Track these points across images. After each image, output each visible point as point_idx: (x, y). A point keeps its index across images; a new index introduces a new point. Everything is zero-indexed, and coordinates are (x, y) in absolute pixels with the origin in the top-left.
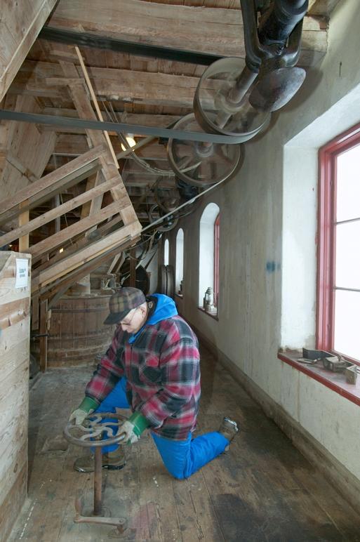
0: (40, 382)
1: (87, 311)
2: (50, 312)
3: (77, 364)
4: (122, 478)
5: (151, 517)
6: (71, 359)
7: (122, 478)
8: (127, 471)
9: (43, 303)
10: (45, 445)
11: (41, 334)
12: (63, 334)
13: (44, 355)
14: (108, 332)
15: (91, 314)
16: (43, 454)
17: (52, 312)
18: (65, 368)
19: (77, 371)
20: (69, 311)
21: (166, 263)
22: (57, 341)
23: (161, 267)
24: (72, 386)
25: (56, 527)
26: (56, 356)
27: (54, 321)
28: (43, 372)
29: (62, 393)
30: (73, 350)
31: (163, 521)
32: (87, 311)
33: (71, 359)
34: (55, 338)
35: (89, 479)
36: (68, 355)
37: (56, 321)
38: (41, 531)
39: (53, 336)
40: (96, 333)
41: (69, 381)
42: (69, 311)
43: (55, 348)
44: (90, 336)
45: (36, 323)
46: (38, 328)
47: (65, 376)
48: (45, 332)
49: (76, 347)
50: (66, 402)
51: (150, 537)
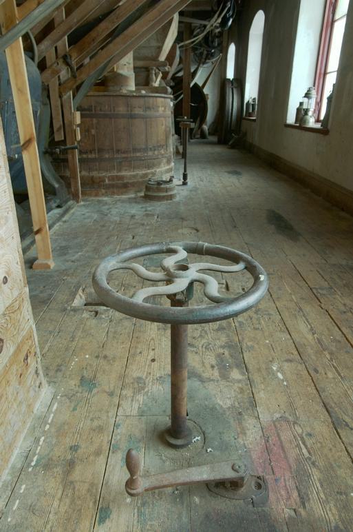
0: (73, 213)
1: (132, 117)
2: (78, 114)
3: (122, 194)
4: (214, 363)
5: (292, 454)
6: (113, 186)
7: (214, 363)
8: (221, 351)
9: (65, 97)
10: (78, 296)
11: (68, 146)
12: (100, 151)
13: (76, 178)
14: (162, 152)
15: (137, 122)
16: (75, 310)
17: (82, 116)
18: (105, 199)
19: (123, 201)
20: (105, 116)
21: (230, 74)
22: (94, 160)
23: (223, 82)
24: (117, 219)
25: (98, 453)
26: (93, 182)
27: (86, 130)
28: (78, 202)
29: (103, 226)
30: (115, 173)
31: (321, 463)
32: (132, 117)
33: (113, 186)
34: (90, 156)
35: (153, 360)
36: (109, 180)
37: (88, 131)
38: (69, 457)
39: (86, 153)
40: (146, 150)
41: (112, 213)
42: (105, 116)
43: (90, 170)
44: (138, 154)
45: (59, 129)
46: (63, 138)
47: (107, 207)
48: (73, 143)
49: (120, 170)
50: (107, 238)
51: (303, 504)
